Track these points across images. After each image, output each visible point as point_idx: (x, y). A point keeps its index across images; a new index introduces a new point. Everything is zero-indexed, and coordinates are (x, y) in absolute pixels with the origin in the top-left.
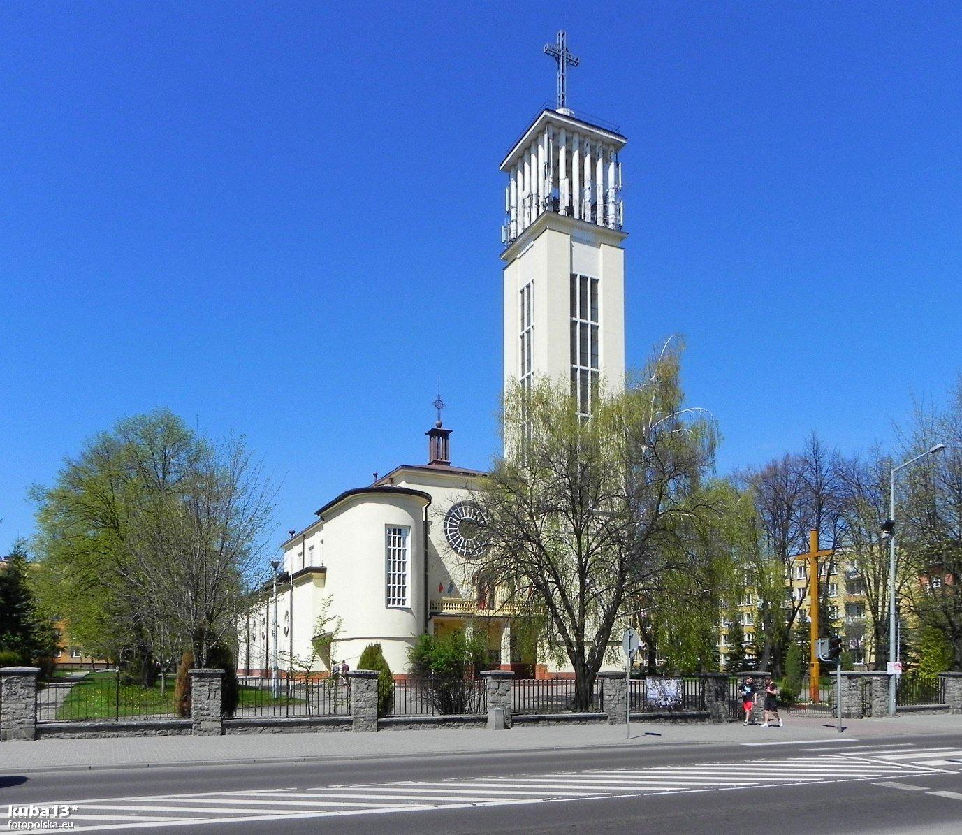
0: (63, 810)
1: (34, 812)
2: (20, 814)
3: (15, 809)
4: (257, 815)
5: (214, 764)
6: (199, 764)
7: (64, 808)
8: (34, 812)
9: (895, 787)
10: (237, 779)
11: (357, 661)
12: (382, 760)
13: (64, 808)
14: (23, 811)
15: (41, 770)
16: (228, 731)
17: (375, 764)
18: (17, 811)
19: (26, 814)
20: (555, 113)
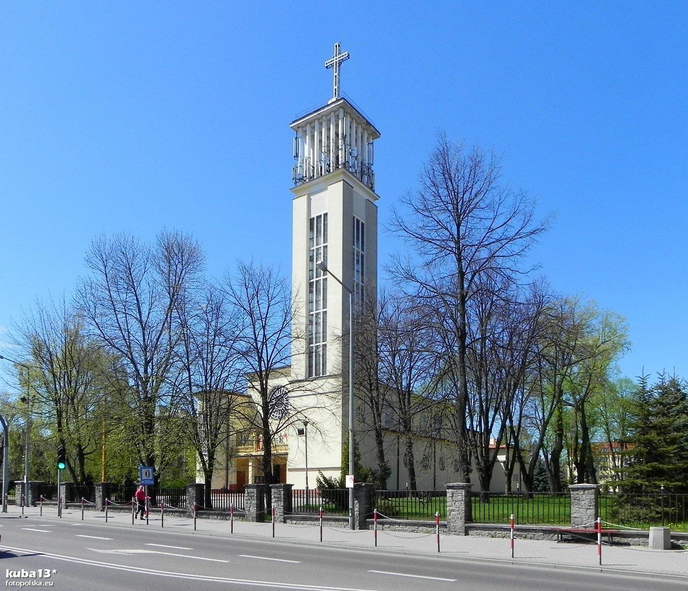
0: (46, 573)
1: (25, 574)
2: (15, 576)
3: (11, 572)
4: (153, 572)
5: (419, 555)
6: (402, 553)
7: (46, 571)
8: (25, 574)
9: (107, 551)
10: (381, 563)
11: (296, 489)
12: (462, 561)
13: (46, 571)
14: (16, 574)
15: (414, 555)
16: (288, 521)
17: (532, 570)
18: (12, 574)
19: (18, 576)
20: (328, 105)
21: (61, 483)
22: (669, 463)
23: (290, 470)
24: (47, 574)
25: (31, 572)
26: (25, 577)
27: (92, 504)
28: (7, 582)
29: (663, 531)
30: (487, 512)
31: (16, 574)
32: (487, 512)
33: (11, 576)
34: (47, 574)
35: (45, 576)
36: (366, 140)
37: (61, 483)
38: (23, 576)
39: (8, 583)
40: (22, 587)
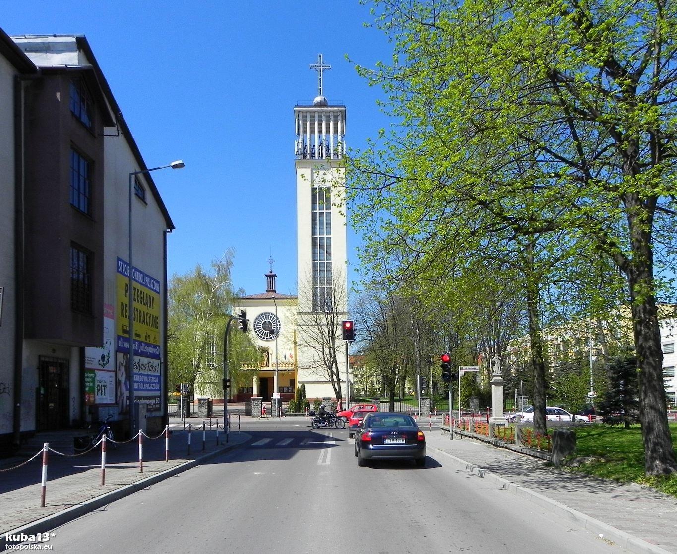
0: (45, 536)
1: (24, 538)
2: (15, 539)
8: (24, 538)
19: (18, 539)
21: (317, 115)
22: (204, 349)
23: (171, 423)
24: (46, 538)
25: (30, 536)
26: (24, 540)
27: (43, 359)
28: (7, 545)
29: (169, 422)
30: (312, 139)
31: (16, 537)
32: (312, 139)
33: (11, 540)
34: (46, 538)
35: (44, 539)
36: (263, 311)
37: (317, 115)
38: (22, 539)
39: (8, 546)
40: (21, 550)
